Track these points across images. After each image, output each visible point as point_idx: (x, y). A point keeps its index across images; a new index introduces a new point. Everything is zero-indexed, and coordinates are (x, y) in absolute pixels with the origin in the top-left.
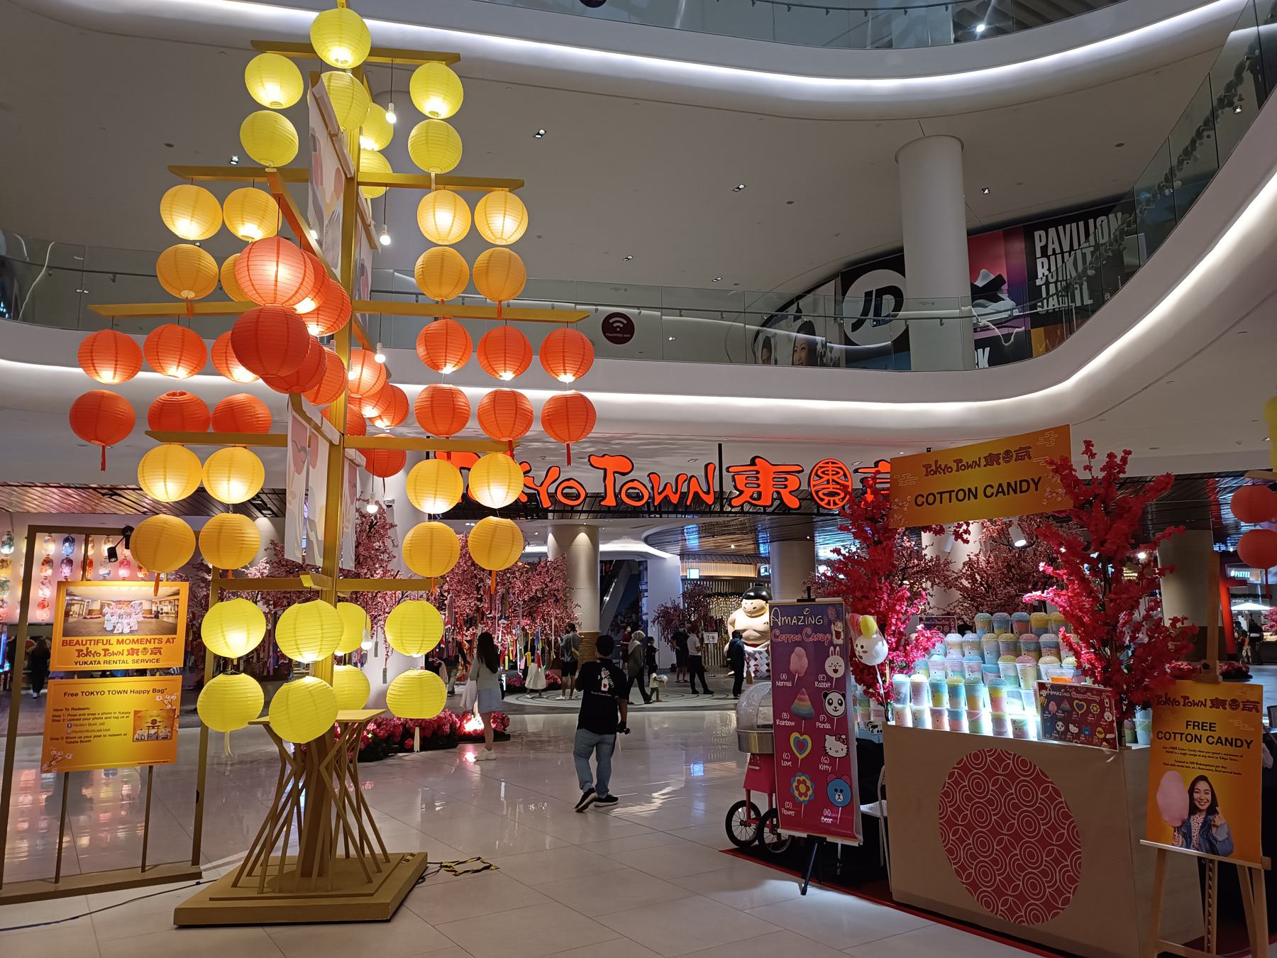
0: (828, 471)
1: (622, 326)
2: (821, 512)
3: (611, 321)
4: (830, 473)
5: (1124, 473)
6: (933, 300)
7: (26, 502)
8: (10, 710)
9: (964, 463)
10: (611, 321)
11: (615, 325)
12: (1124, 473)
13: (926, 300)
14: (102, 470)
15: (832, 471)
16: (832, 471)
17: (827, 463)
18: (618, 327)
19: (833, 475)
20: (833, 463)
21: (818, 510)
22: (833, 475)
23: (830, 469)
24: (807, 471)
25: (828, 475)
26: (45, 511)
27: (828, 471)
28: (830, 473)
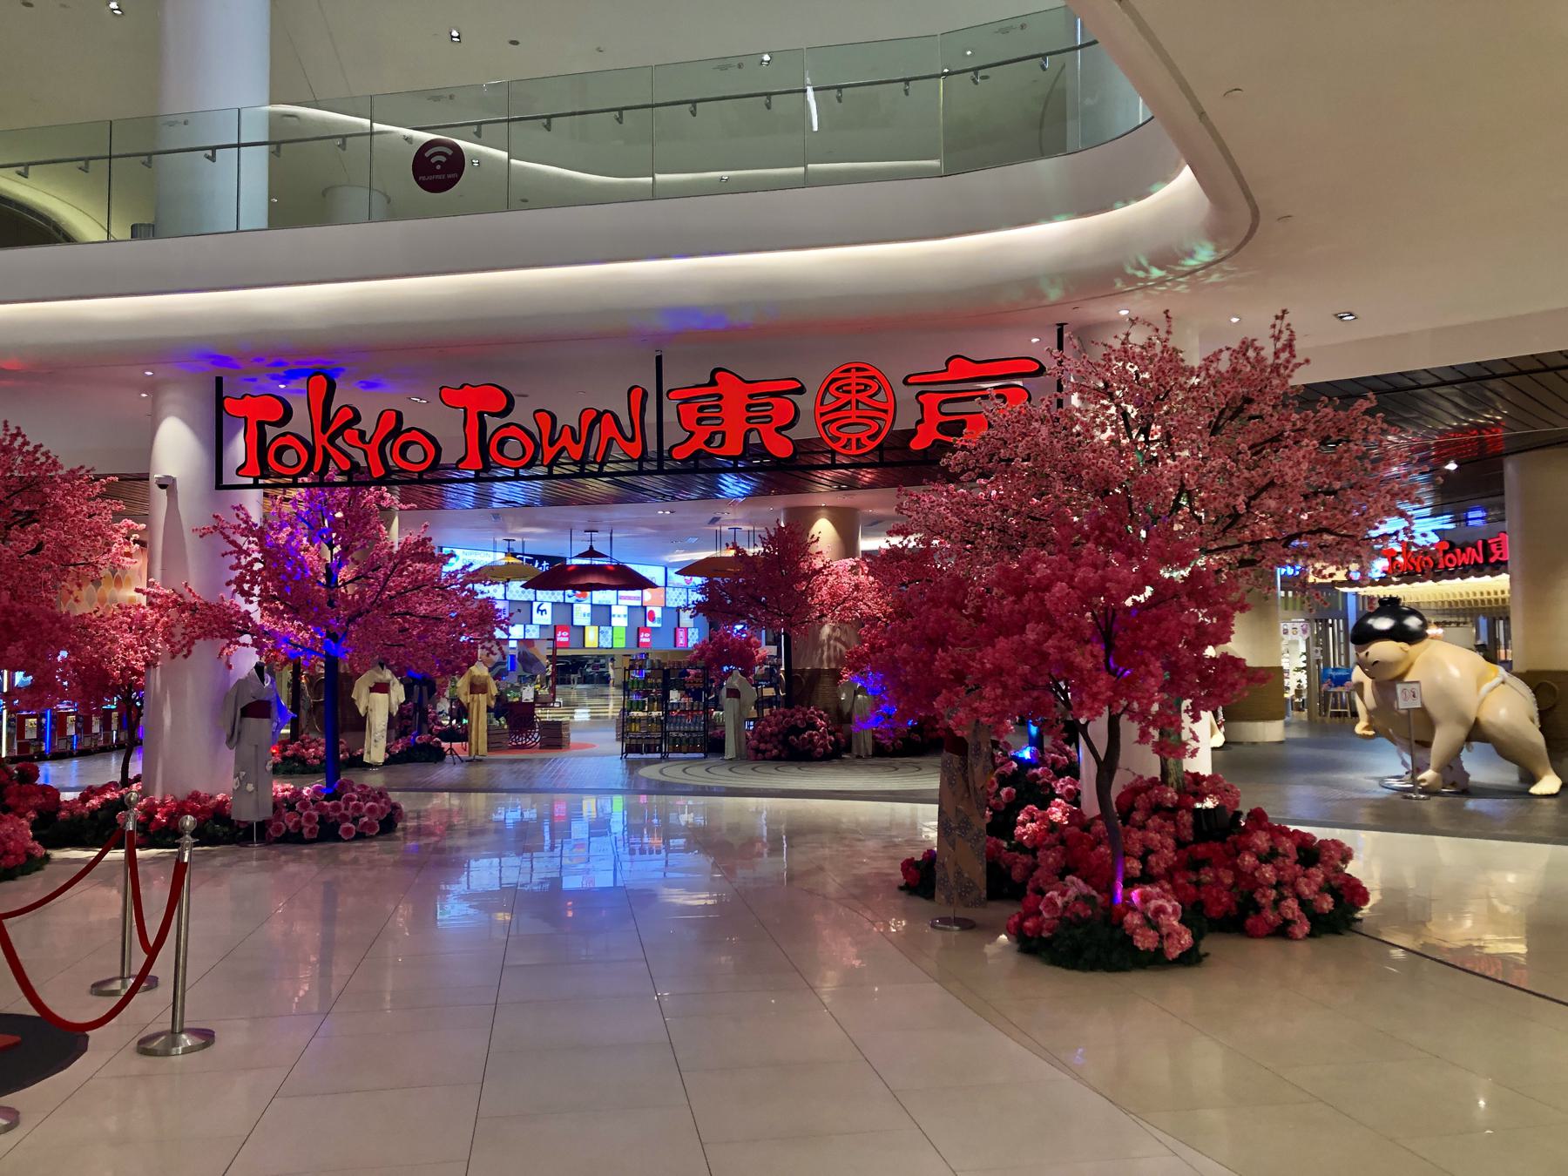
0: (849, 384)
1: (443, 159)
2: (555, 472)
3: (427, 154)
4: (854, 388)
5: (61, 467)
6: (1021, 21)
7: (1438, 412)
8: (37, 1017)
9: (522, 415)
10: (427, 154)
11: (433, 160)
12: (61, 467)
13: (1006, 24)
14: (221, 378)
15: (857, 384)
16: (857, 384)
17: (848, 370)
18: (439, 162)
19: (858, 391)
20: (858, 369)
21: (833, 459)
22: (858, 391)
23: (854, 381)
24: (813, 388)
25: (849, 392)
26: (793, 473)
27: (849, 384)
28: (854, 388)
